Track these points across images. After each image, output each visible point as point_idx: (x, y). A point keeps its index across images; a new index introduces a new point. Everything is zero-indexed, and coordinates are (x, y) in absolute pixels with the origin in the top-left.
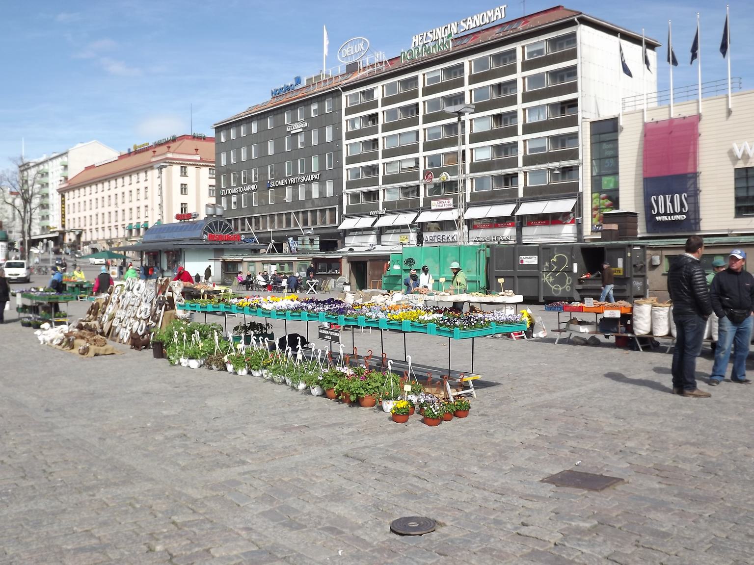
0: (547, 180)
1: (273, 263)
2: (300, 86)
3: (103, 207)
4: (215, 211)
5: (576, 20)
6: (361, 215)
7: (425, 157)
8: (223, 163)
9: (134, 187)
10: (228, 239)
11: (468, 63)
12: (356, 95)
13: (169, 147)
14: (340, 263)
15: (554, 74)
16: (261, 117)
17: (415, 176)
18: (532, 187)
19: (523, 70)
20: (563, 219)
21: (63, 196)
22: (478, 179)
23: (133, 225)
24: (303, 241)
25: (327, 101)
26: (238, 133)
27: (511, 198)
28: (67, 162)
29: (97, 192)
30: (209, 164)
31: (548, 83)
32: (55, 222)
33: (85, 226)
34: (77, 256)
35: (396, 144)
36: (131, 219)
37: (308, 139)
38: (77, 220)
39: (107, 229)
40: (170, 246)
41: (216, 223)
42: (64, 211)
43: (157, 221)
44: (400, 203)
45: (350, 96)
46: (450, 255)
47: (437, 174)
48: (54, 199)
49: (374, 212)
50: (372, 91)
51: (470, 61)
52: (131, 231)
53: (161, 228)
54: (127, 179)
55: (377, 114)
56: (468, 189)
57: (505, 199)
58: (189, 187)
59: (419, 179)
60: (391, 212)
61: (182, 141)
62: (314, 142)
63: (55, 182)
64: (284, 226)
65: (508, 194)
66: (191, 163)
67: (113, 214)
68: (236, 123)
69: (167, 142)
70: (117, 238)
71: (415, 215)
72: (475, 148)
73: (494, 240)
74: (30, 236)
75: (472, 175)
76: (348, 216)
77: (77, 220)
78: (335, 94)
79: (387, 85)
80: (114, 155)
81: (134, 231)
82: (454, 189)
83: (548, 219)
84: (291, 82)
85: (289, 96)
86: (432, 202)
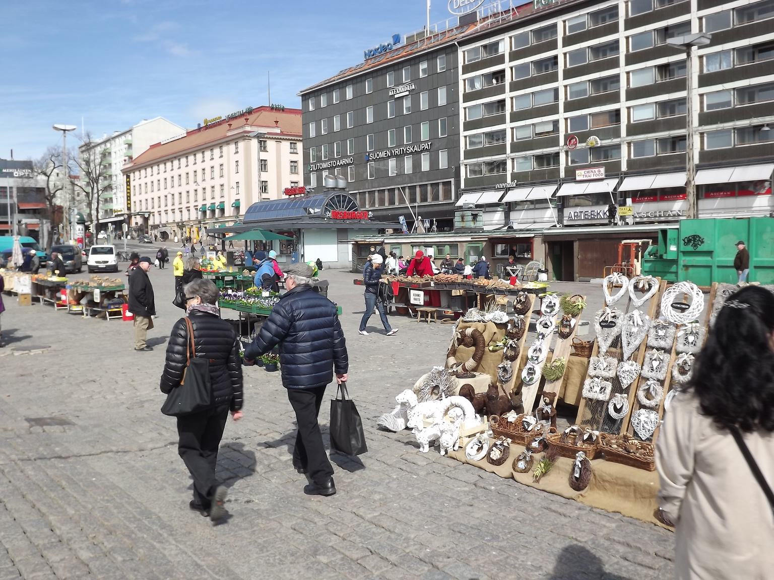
2: (399, 46)
3: (140, 194)
4: (337, 182)
5: (456, 43)
6: (484, 189)
7: (566, 119)
8: (312, 134)
9: (191, 169)
10: (353, 217)
12: (477, 49)
13: (247, 120)
14: (532, 243)
15: (596, 50)
16: (356, 80)
17: (555, 142)
18: (637, 160)
19: (626, 29)
20: (755, 188)
21: (128, 177)
23: (207, 206)
24: (463, 217)
25: (439, 59)
26: (330, 100)
27: (679, 165)
28: (132, 141)
29: (146, 177)
30: (290, 138)
31: (590, 59)
32: (119, 204)
33: (153, 208)
34: (146, 240)
35: (528, 105)
36: (204, 200)
38: (144, 202)
39: (177, 211)
40: (285, 225)
41: (338, 196)
42: (130, 193)
43: (234, 201)
44: (534, 174)
45: (468, 51)
46: (769, 229)
47: (583, 138)
49: (501, 186)
52: (204, 212)
55: (503, 71)
56: (624, 156)
57: (675, 166)
58: (269, 164)
59: (506, 154)
60: (523, 184)
61: (258, 114)
62: (424, 105)
63: (118, 163)
64: (387, 204)
65: (678, 161)
66: (271, 136)
67: (192, 193)
68: (328, 89)
70: (189, 220)
71: (554, 187)
72: (633, 107)
73: (660, 216)
74: (98, 220)
75: (630, 138)
76: (467, 191)
77: (144, 202)
78: (451, 49)
79: (516, 37)
80: (181, 132)
82: (501, 169)
84: (388, 41)
85: (389, 56)
86: (577, 172)
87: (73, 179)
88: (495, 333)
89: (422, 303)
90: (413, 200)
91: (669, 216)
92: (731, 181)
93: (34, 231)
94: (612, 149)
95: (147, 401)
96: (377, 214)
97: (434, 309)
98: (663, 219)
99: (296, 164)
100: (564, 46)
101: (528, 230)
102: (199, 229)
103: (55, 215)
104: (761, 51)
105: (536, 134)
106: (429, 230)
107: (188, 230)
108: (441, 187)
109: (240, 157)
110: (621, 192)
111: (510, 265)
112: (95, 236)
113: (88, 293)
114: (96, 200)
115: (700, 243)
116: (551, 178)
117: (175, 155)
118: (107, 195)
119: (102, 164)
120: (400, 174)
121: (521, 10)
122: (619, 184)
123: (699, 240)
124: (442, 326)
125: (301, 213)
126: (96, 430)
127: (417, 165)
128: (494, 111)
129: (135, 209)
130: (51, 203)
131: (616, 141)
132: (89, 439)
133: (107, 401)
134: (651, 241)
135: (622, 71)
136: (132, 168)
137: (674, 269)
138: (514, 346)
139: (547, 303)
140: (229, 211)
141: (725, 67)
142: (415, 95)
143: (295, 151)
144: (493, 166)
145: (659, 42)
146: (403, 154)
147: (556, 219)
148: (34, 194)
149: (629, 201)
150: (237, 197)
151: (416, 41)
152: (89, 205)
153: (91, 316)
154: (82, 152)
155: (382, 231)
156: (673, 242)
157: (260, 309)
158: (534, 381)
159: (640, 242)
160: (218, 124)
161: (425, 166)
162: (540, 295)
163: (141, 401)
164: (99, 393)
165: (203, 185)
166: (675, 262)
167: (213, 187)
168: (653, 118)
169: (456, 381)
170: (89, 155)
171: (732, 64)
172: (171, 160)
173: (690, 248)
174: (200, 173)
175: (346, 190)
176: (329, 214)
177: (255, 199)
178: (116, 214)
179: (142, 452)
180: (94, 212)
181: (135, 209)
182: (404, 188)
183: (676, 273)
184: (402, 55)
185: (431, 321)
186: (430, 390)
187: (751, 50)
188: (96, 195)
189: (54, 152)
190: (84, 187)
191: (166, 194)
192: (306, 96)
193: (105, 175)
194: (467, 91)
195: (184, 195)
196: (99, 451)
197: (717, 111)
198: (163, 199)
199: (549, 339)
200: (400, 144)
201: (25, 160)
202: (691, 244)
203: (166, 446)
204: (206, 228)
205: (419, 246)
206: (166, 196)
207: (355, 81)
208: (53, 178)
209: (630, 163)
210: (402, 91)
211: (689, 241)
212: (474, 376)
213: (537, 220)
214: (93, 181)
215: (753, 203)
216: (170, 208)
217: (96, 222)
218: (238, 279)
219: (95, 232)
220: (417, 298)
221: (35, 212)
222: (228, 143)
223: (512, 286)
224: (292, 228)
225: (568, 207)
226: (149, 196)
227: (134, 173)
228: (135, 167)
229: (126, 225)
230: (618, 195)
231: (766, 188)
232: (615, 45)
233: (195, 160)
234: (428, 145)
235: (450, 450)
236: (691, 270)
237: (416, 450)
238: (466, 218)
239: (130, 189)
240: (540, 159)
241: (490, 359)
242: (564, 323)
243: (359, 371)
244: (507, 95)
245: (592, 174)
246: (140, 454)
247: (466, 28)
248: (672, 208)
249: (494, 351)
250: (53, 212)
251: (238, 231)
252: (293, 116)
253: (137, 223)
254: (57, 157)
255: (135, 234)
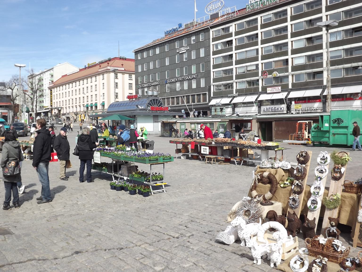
0: (343, 75)
1: (198, 123)
2: (181, 29)
4: (153, 93)
5: (209, 27)
6: (222, 97)
7: (262, 64)
8: (140, 70)
11: (290, 9)
12: (219, 30)
13: (108, 63)
15: (276, 30)
16: (161, 45)
17: (257, 74)
19: (291, 21)
20: (354, 97)
21: (51, 91)
22: (296, 75)
23: (89, 105)
24: (215, 110)
26: (148, 54)
27: (319, 85)
28: (53, 73)
29: (60, 91)
30: (129, 72)
31: (274, 35)
32: (47, 104)
33: (63, 105)
35: (243, 57)
37: (190, 56)
38: (58, 103)
39: (74, 107)
41: (154, 100)
42: (52, 98)
43: (102, 102)
44: (246, 90)
45: (215, 31)
47: (271, 72)
48: (47, 92)
49: (231, 95)
50: (229, 28)
51: (291, 8)
52: (88, 108)
53: (119, 104)
54: (71, 85)
55: (232, 41)
60: (241, 95)
61: (114, 61)
62: (193, 57)
63: (46, 84)
64: (175, 104)
65: (316, 83)
67: (82, 99)
68: (147, 49)
69: (106, 61)
72: (295, 58)
73: (308, 110)
74: (36, 111)
75: (293, 73)
76: (214, 98)
77: (58, 103)
78: (206, 30)
80: (77, 70)
81: (89, 108)
83: (306, 100)
85: (177, 33)
86: (268, 89)
87: (25, 92)
88: (283, 176)
89: (208, 153)
90: (188, 102)
91: (312, 110)
92: (342, 93)
93: (5, 116)
94: (284, 78)
95: (60, 215)
96: (172, 108)
97: (215, 157)
98: (309, 111)
99: (131, 85)
100: (261, 29)
101: (249, 116)
102: (85, 116)
103: (15, 108)
104: (356, 31)
105: (248, 71)
106: (198, 116)
107: (79, 116)
108: (201, 96)
109: (105, 81)
110: (289, 98)
111: (242, 133)
112: (35, 118)
113: (29, 147)
114: (36, 102)
115: (341, 122)
116: (255, 92)
117: (74, 80)
118: (41, 99)
119: (39, 84)
120: (182, 90)
121: (240, 12)
122: (288, 95)
123: (341, 121)
124: (220, 166)
125: (135, 108)
126: (26, 239)
127: (190, 85)
128: (227, 60)
129: (54, 106)
130: (13, 103)
131: (286, 74)
132: (20, 248)
133: (35, 215)
134: (312, 121)
135: (289, 41)
136: (53, 86)
137: (327, 135)
138: (300, 184)
139: (322, 157)
140: (99, 107)
141: (339, 39)
142: (189, 52)
143: (131, 79)
144: (226, 86)
145: (307, 27)
146: (183, 80)
147: (257, 112)
148: (5, 98)
149: (293, 103)
150: (103, 100)
151: (189, 26)
152: (32, 104)
153: (30, 159)
154: (29, 79)
155: (174, 117)
156: (327, 122)
157: (126, 157)
158: (317, 208)
159: (307, 122)
160: (95, 65)
161: (194, 86)
162: (276, 149)
163: (56, 215)
164: (30, 209)
165: (87, 94)
166: (328, 132)
167: (92, 96)
168: (304, 63)
169: (262, 207)
170: (33, 79)
171: (342, 37)
172: (72, 83)
173: (336, 125)
174: (85, 89)
175: (157, 96)
176: (149, 108)
177: (112, 101)
178: (45, 108)
179: (56, 260)
180: (34, 107)
181: (54, 106)
182: (184, 96)
183: (329, 137)
184: (183, 33)
185: (213, 163)
186: (244, 213)
187: (351, 31)
188: (35, 99)
189: (15, 78)
190: (30, 95)
191: (69, 99)
192: (137, 53)
193: (40, 89)
194: (214, 50)
195: (78, 99)
196: (26, 259)
197: (338, 59)
198: (68, 101)
199: (324, 180)
200: (182, 75)
201: (2, 82)
202: (336, 123)
203: (72, 255)
204: (88, 115)
205: (194, 124)
206: (69, 100)
207: (160, 45)
208: (15, 91)
209: (293, 84)
210: (183, 50)
211: (336, 121)
212: (272, 204)
213: (248, 112)
214: (34, 92)
215: (353, 104)
216: (71, 105)
217: (35, 112)
218: (107, 140)
219: (35, 116)
220: (205, 150)
221: (6, 107)
222: (99, 75)
223: (259, 145)
224: (131, 114)
225: (263, 105)
226: (61, 100)
227: (54, 89)
228: (55, 86)
229: (50, 113)
230: (287, 100)
231: (359, 97)
232: (286, 28)
233: (83, 82)
234: (195, 76)
235: (278, 264)
236: (336, 136)
237: (251, 262)
238: (217, 110)
239: (52, 96)
240: (249, 83)
241: (281, 193)
242: (336, 170)
243: (184, 194)
244: (234, 52)
245: (275, 90)
246: (54, 262)
247: (213, 20)
248: (314, 106)
249: (284, 187)
250: (15, 107)
251: (104, 116)
252: (130, 62)
253: (55, 113)
254: (16, 80)
255: (54, 118)
